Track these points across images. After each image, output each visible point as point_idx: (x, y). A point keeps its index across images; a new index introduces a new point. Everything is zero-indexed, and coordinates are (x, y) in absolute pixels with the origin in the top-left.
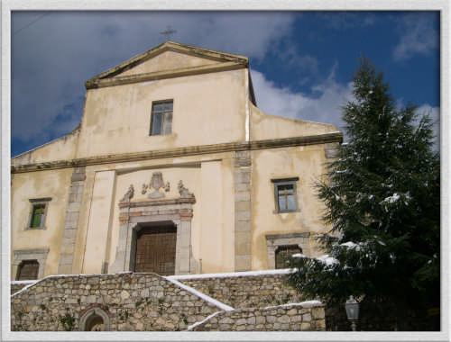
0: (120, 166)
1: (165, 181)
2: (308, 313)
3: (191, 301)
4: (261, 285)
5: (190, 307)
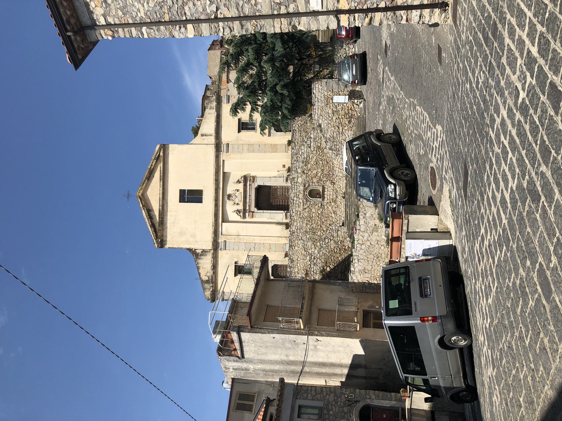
3: (304, 149)
4: (295, 130)
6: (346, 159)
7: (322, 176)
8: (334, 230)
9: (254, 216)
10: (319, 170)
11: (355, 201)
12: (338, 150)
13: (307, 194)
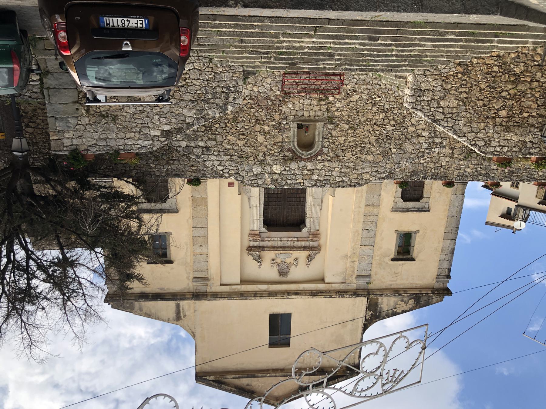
0: (321, 286)
1: (275, 269)
2: (66, 147)
3: (212, 161)
5: (213, 154)
6: (454, 36)
7: (271, 123)
8: (418, 99)
9: (315, 233)
10: (258, 128)
11: (382, 45)
12: (225, 90)
13: (305, 153)
